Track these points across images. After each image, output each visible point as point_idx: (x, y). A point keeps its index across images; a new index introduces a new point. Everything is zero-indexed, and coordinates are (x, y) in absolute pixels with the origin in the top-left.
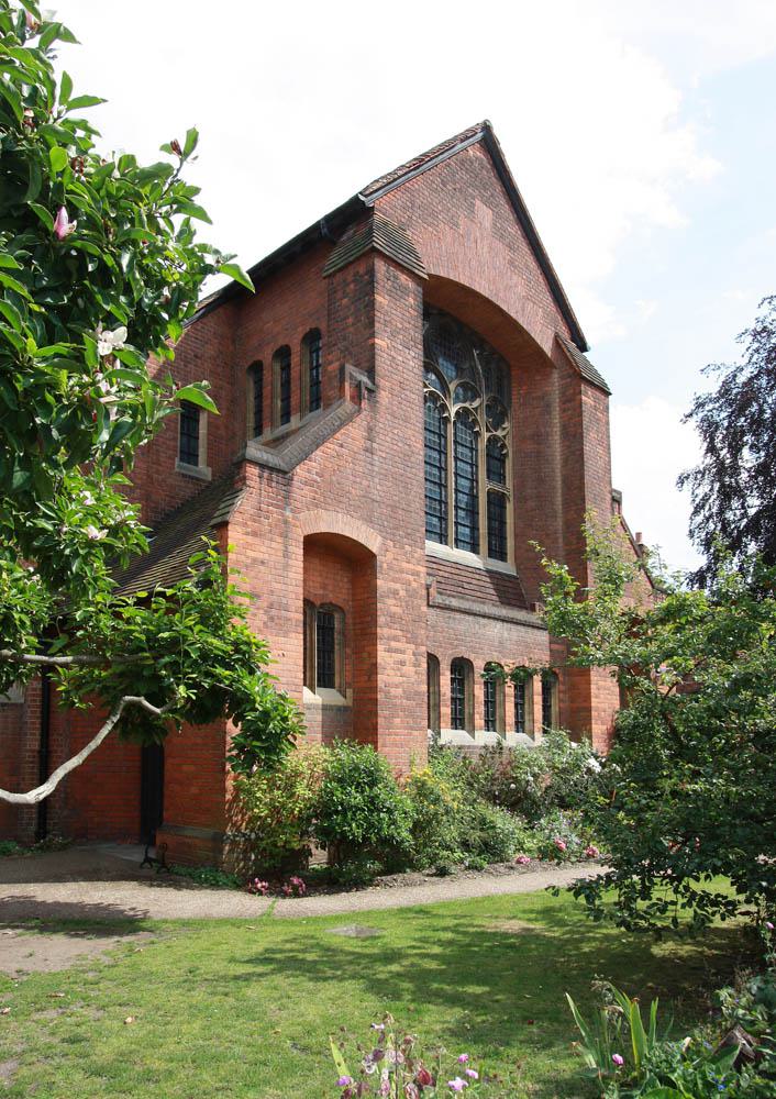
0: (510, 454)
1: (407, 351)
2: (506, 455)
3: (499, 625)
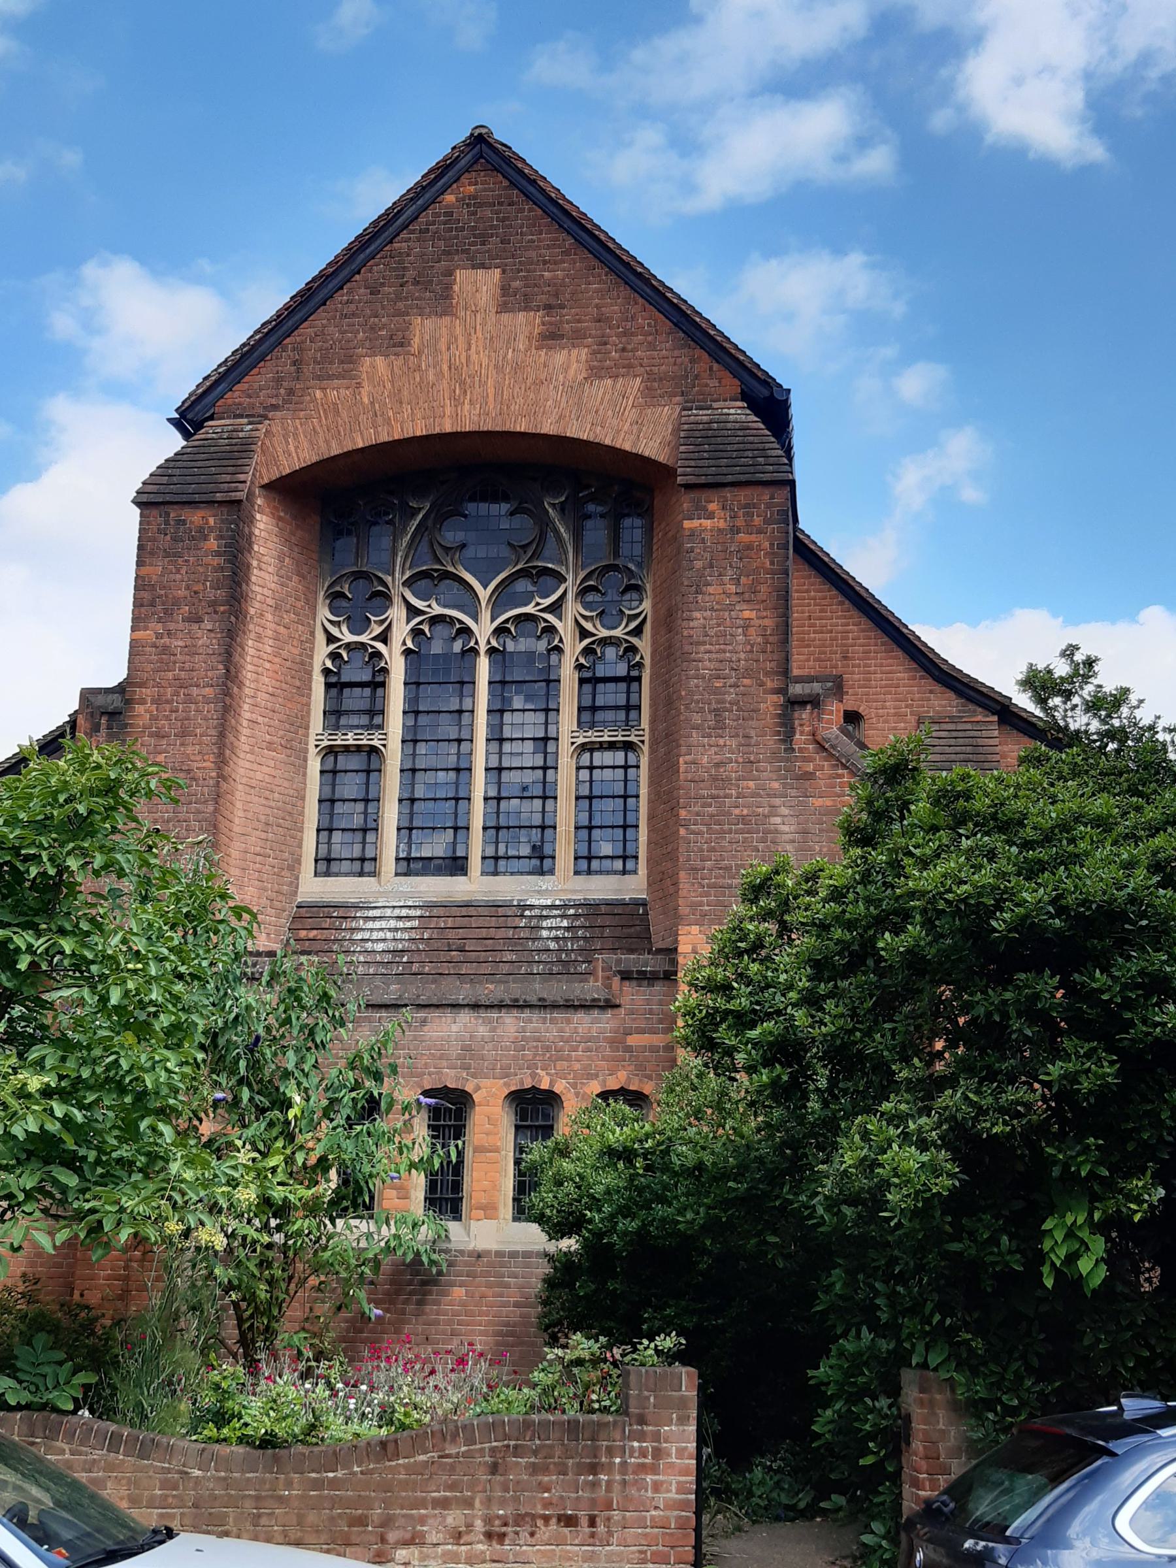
0: (647, 662)
1: (195, 626)
2: (640, 665)
3: (465, 1017)
